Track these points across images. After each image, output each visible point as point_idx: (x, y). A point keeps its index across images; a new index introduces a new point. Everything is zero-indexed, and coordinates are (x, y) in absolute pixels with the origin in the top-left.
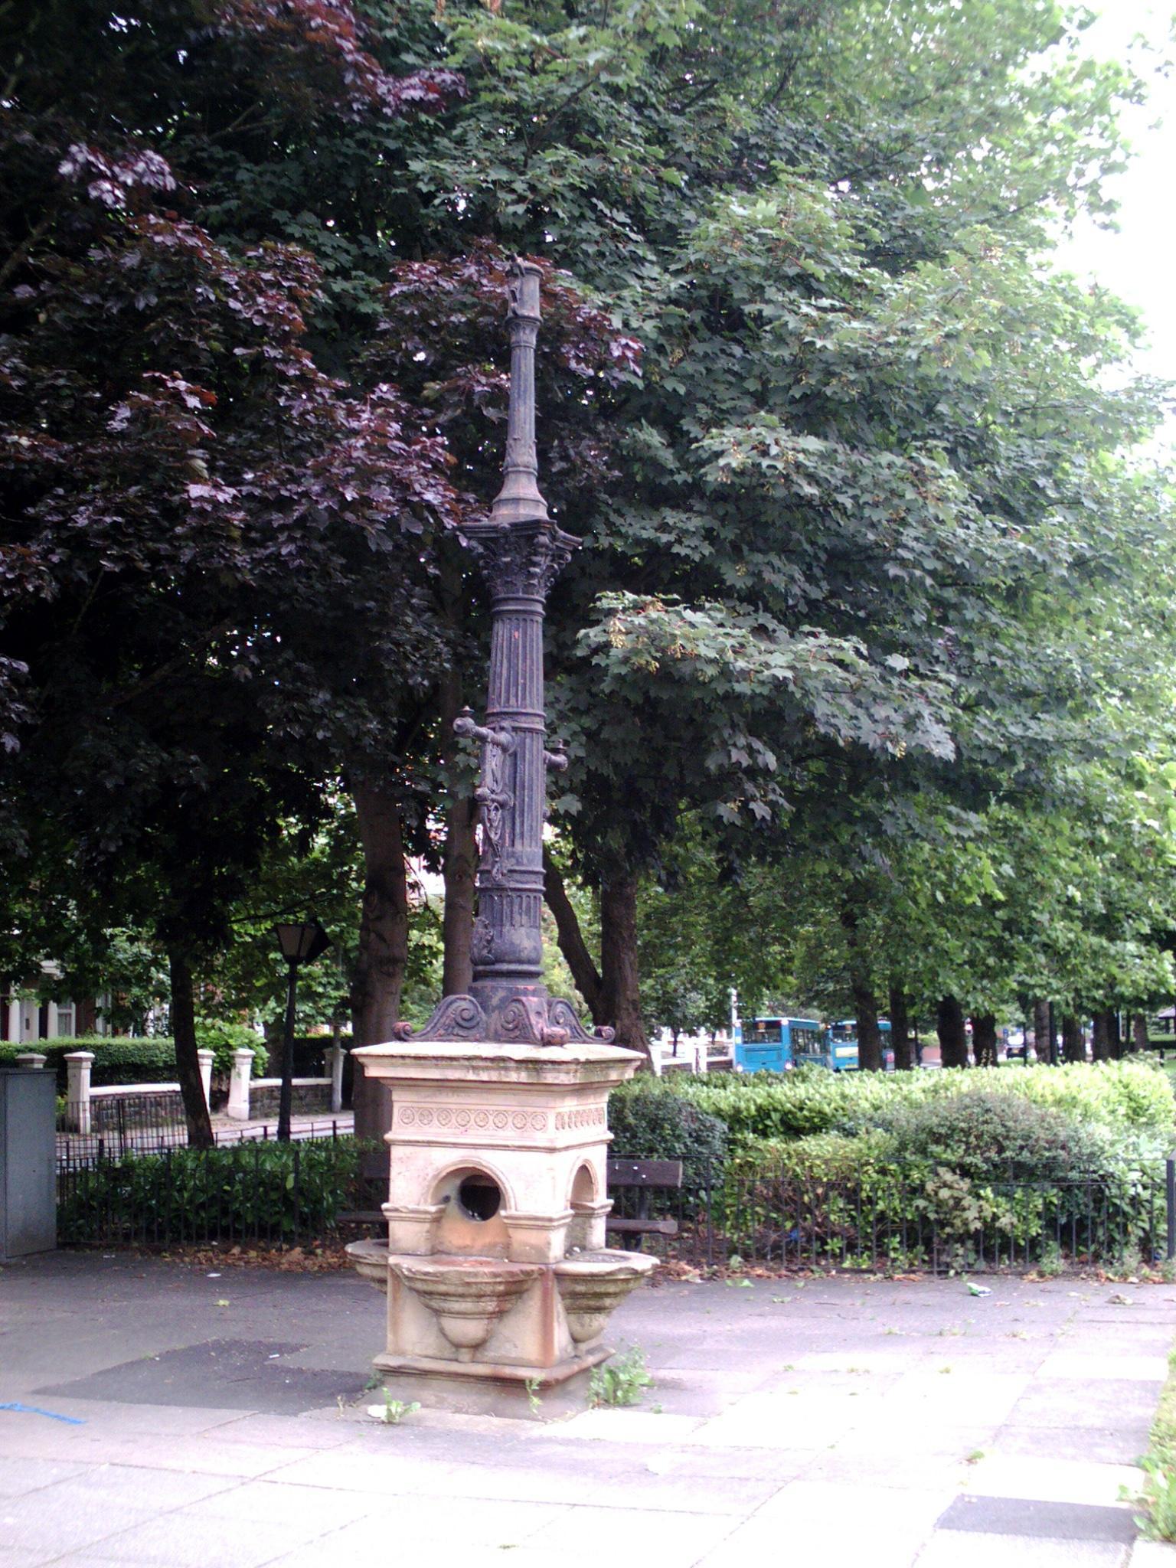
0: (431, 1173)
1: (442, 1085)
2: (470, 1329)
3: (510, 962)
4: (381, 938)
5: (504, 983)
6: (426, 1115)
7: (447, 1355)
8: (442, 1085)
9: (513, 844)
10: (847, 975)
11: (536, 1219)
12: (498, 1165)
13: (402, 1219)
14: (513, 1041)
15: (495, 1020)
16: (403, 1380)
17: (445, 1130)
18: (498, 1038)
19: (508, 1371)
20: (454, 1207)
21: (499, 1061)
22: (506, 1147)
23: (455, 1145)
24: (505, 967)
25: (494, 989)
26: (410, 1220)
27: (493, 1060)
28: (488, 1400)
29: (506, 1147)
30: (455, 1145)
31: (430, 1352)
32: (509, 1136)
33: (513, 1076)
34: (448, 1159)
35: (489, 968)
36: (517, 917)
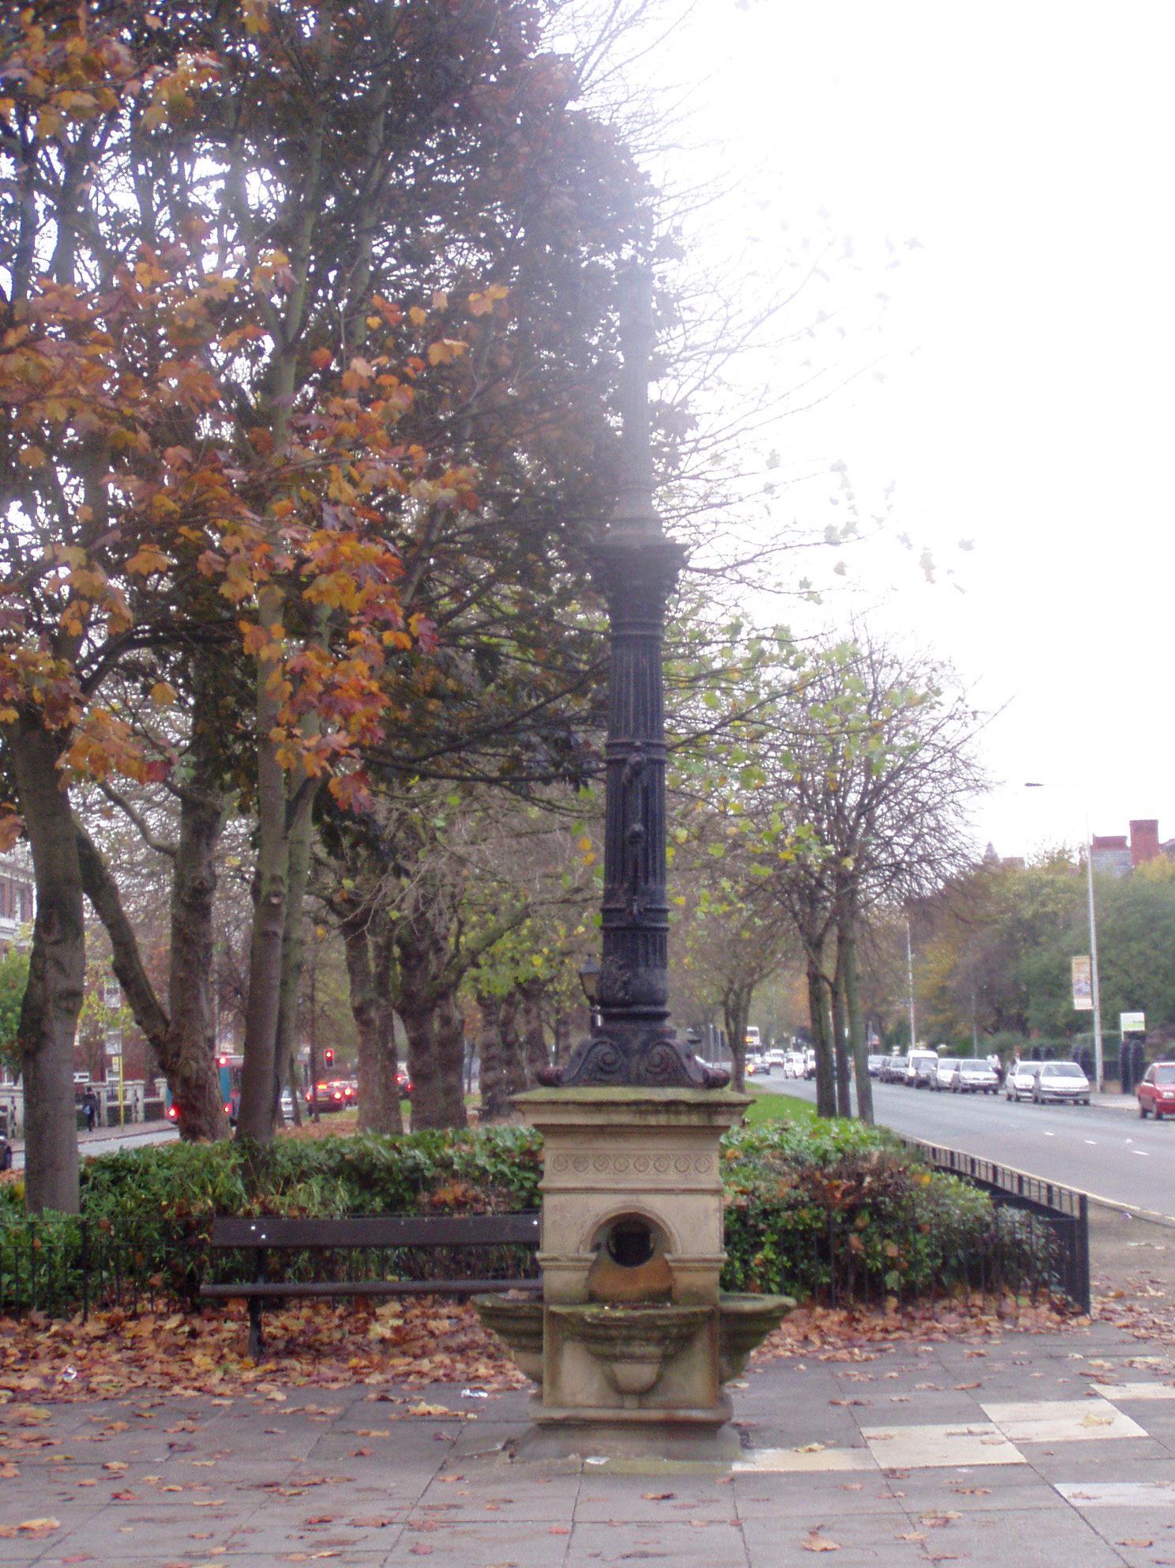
0: (589, 1223)
1: (600, 1131)
2: (641, 1373)
3: (645, 1004)
4: (58, 964)
5: (644, 1027)
6: (579, 1163)
7: (611, 1402)
8: (600, 1131)
9: (646, 882)
10: (356, 752)
11: (705, 1260)
12: (656, 1206)
13: (559, 1268)
14: (662, 1084)
15: (637, 1064)
16: (562, 1433)
17: (603, 1176)
18: (640, 1082)
19: (682, 1414)
20: (607, 1258)
21: (670, 1106)
22: (670, 1191)
23: (615, 1191)
24: (645, 1009)
25: (635, 1034)
26: (568, 1268)
27: (628, 1104)
28: (661, 1444)
29: (670, 1191)
30: (615, 1191)
31: (592, 1402)
32: (672, 1179)
33: (684, 1120)
34: (608, 1206)
35: (846, 1020)
36: (651, 956)
